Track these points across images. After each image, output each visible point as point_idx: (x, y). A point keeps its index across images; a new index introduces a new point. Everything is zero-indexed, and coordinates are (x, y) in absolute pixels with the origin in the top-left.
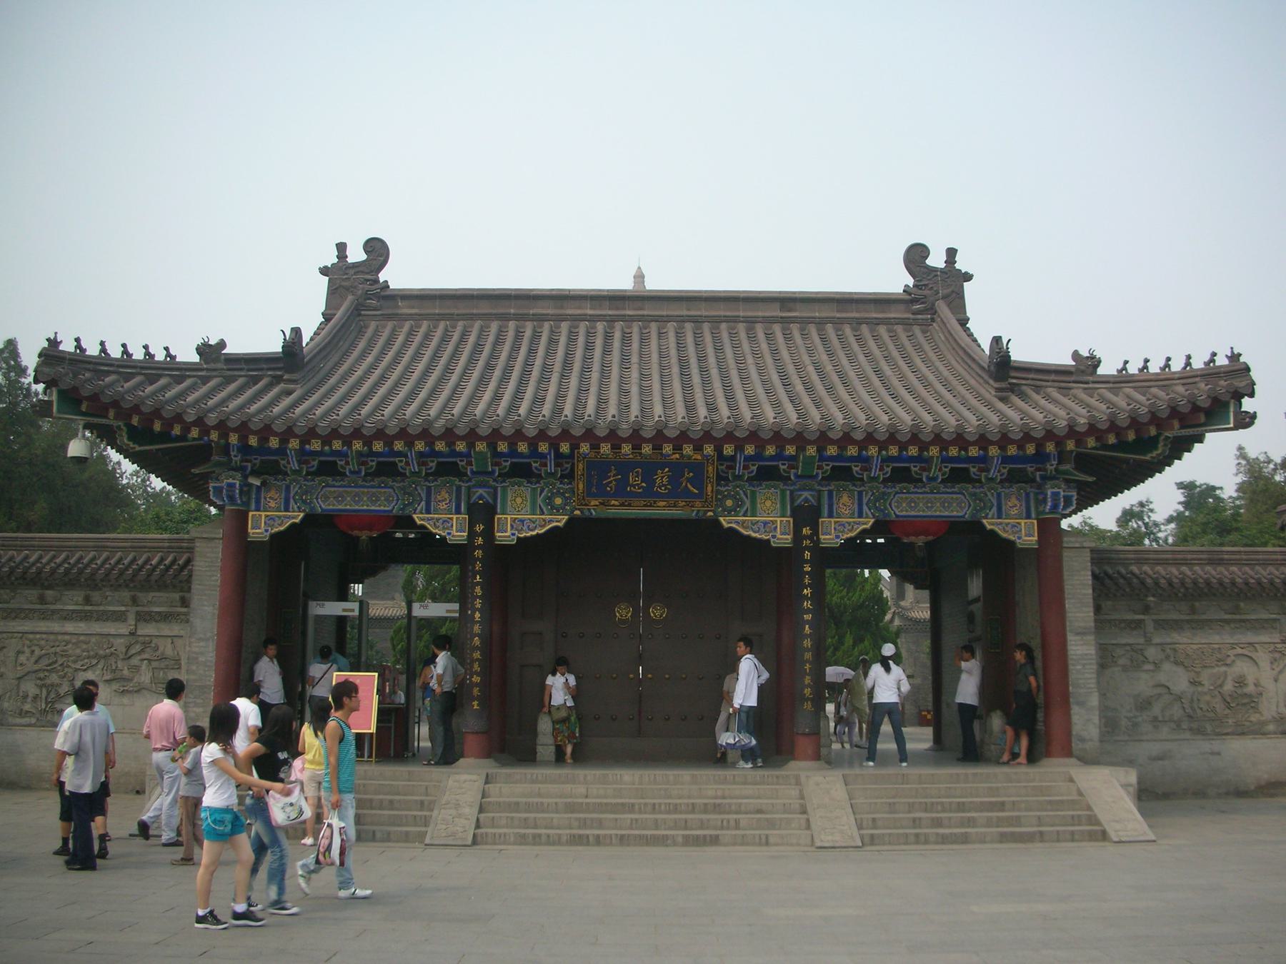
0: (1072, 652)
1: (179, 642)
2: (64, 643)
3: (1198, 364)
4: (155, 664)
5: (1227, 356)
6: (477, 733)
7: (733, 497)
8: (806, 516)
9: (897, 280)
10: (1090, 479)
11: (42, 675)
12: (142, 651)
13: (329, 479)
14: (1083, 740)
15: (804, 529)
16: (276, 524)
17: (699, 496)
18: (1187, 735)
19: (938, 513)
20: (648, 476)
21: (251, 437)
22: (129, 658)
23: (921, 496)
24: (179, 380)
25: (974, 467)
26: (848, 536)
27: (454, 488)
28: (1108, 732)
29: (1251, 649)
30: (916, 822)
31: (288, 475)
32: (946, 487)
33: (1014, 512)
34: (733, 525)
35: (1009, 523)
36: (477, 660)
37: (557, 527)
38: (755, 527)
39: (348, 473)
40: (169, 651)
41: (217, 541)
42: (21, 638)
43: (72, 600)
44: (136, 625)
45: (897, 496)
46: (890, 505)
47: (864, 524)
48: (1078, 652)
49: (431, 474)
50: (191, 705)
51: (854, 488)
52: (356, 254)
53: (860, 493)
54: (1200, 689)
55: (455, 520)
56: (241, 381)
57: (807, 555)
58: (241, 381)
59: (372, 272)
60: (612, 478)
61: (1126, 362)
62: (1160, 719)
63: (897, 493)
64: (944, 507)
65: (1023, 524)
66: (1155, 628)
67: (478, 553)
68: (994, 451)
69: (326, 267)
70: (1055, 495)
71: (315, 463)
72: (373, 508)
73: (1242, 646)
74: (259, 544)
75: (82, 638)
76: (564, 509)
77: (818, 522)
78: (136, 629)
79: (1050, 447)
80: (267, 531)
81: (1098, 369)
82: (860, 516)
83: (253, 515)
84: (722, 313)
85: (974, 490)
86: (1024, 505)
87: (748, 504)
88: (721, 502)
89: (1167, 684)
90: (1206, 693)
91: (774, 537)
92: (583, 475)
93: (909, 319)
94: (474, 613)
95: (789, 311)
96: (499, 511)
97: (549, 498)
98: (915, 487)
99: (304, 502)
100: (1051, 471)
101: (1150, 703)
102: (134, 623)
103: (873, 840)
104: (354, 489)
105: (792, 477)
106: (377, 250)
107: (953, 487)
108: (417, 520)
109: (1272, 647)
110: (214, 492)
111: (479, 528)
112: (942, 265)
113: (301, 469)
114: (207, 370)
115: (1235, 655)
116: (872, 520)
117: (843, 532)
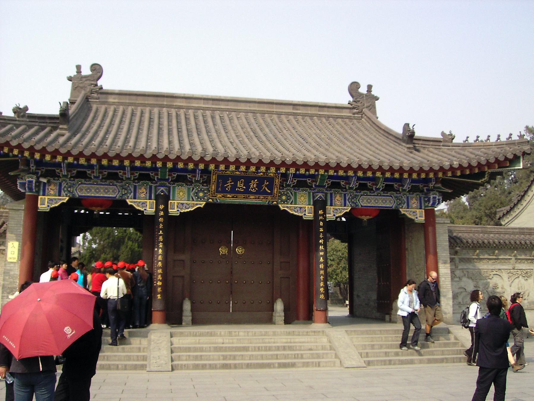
3: (503, 139)
5: (518, 136)
6: (160, 311)
7: (286, 195)
9: (345, 99)
10: (450, 191)
13: (83, 180)
14: (445, 313)
15: (320, 211)
16: (53, 203)
17: (271, 194)
19: (380, 205)
20: (247, 184)
21: (47, 155)
23: (373, 197)
25: (396, 184)
27: (148, 186)
29: (500, 272)
30: (386, 354)
31: (61, 178)
33: (414, 206)
34: (286, 209)
36: (160, 274)
37: (200, 207)
39: (92, 178)
41: (21, 211)
45: (362, 196)
46: (359, 200)
48: (443, 272)
49: (137, 179)
51: (342, 192)
52: (86, 71)
55: (148, 203)
56: (36, 128)
57: (321, 224)
58: (36, 128)
59: (94, 80)
60: (229, 184)
61: (468, 137)
62: (462, 303)
63: (362, 195)
64: (383, 203)
65: (418, 212)
67: (161, 220)
68: (406, 176)
69: (70, 77)
70: (434, 198)
71: (75, 172)
73: (496, 270)
74: (45, 214)
76: (204, 198)
79: (431, 175)
80: (48, 206)
81: (453, 140)
82: (345, 206)
84: (265, 109)
85: (397, 195)
87: (293, 198)
89: (464, 287)
91: (305, 215)
92: (215, 182)
93: (351, 116)
94: (158, 250)
95: (297, 110)
96: (171, 198)
97: (196, 193)
99: (69, 192)
100: (432, 187)
103: (369, 363)
104: (95, 186)
105: (314, 186)
109: (509, 271)
110: (20, 185)
111: (162, 207)
112: (366, 92)
113: (68, 175)
114: (19, 121)
115: (494, 275)
116: (350, 208)
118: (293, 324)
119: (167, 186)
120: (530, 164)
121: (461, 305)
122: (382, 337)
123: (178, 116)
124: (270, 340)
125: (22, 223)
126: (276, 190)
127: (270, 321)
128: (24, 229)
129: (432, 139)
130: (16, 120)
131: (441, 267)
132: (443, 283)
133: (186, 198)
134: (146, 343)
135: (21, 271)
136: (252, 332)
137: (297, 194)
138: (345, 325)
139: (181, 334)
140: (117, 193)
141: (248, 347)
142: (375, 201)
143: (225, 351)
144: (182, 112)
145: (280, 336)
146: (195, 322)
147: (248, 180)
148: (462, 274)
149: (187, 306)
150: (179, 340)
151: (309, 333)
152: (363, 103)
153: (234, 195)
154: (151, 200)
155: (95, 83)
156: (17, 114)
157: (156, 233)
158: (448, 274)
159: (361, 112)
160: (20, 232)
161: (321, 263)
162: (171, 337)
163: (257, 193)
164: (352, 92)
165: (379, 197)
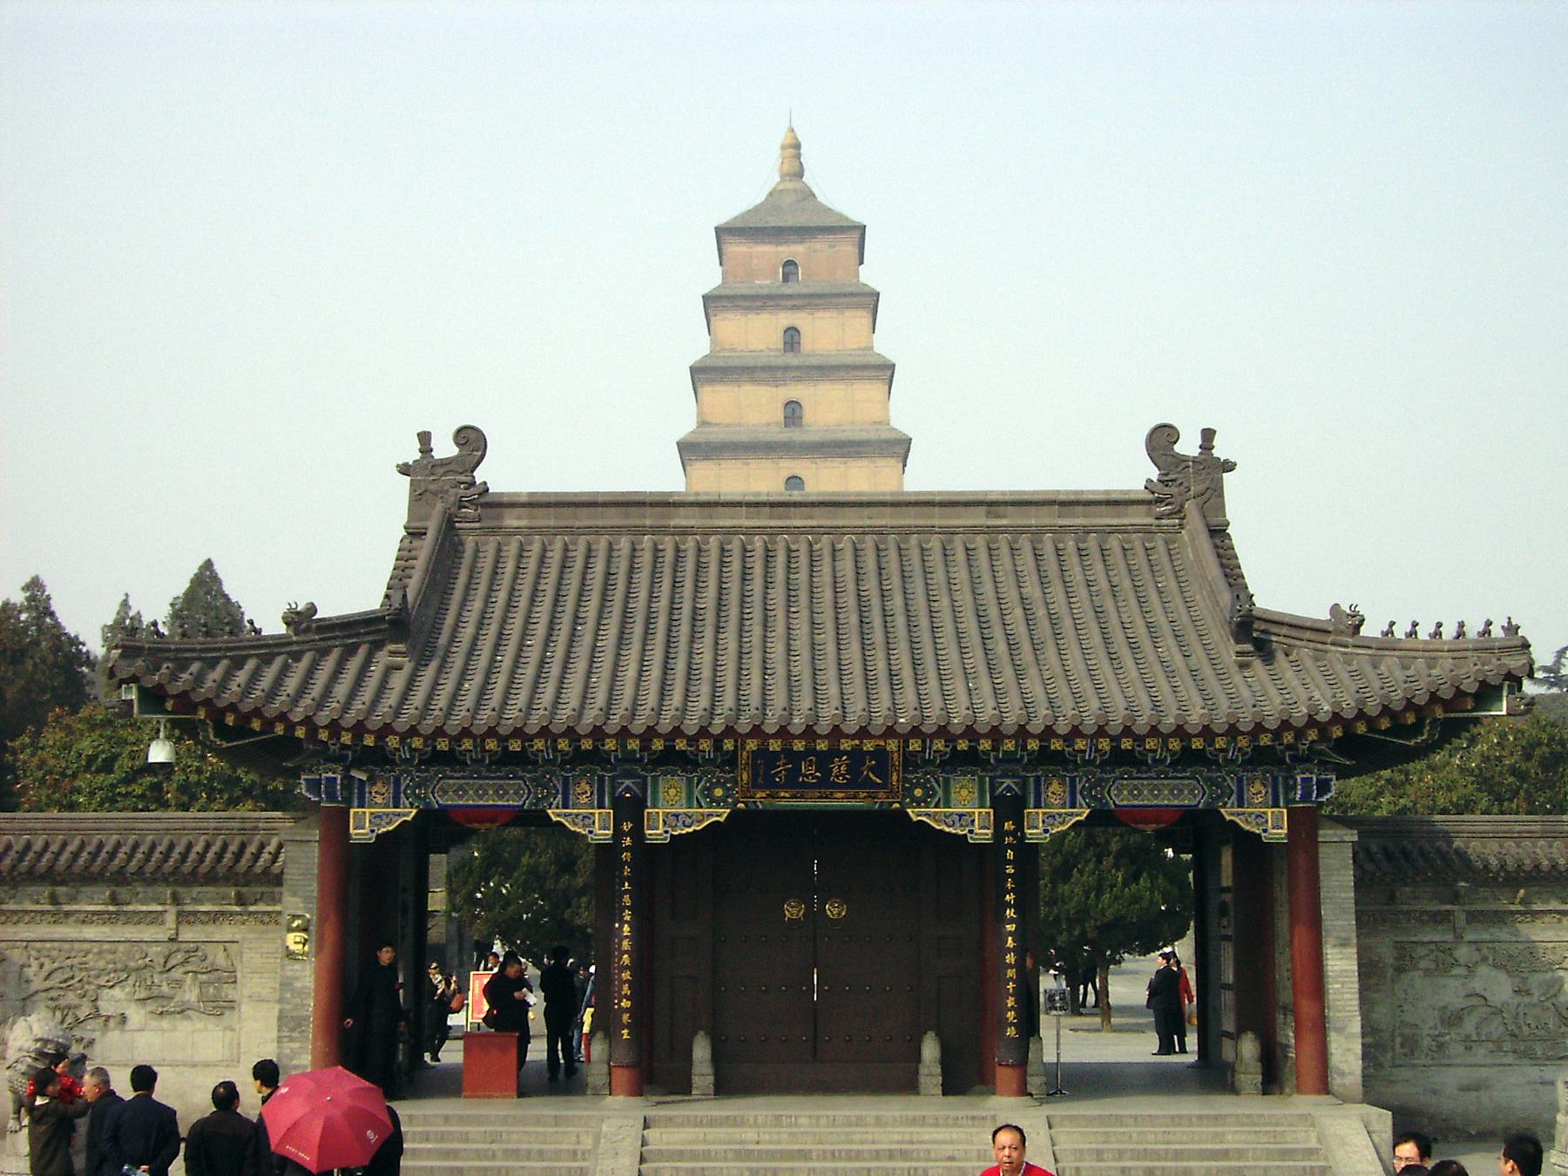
0: (1329, 968)
1: (232, 948)
2: (83, 953)
4: (204, 977)
5: (1503, 627)
6: (627, 1067)
7: (923, 786)
8: (1009, 809)
11: (53, 994)
12: (186, 961)
14: (1342, 1074)
18: (1510, 1059)
22: (170, 970)
24: (267, 660)
26: (1059, 829)
28: (1405, 1055)
31: (397, 765)
32: (1175, 771)
35: (1252, 813)
36: (627, 981)
38: (949, 821)
40: (221, 960)
41: (312, 844)
42: (26, 947)
43: (93, 901)
44: (177, 929)
47: (1077, 815)
48: (1336, 968)
50: (285, 1040)
52: (444, 448)
53: (1073, 780)
54: (1527, 1000)
55: (597, 815)
57: (1010, 854)
60: (782, 768)
64: (1173, 794)
66: (1469, 922)
67: (626, 856)
69: (406, 465)
72: (500, 803)
75: (106, 946)
77: (1023, 813)
78: (177, 934)
80: (373, 831)
81: (1362, 629)
82: (1073, 806)
83: (355, 813)
84: (912, 522)
86: (1270, 790)
88: (908, 792)
89: (1483, 993)
90: (1534, 1006)
91: (971, 832)
94: (621, 927)
97: (708, 789)
98: (1139, 772)
99: (418, 797)
101: (1460, 1018)
102: (174, 926)
106: (471, 441)
107: (1185, 771)
108: (552, 816)
114: (297, 642)
116: (1088, 811)
117: (1053, 824)
118: (970, 1095)
119: (639, 777)
120: (1526, 705)
121: (1472, 1044)
122: (1130, 1133)
123: (678, 552)
124: (864, 1137)
125: (316, 871)
126: (895, 777)
127: (908, 1085)
128: (321, 884)
129: (1308, 624)
130: (291, 644)
131: (1331, 954)
132: (1335, 997)
133: (684, 801)
134: (590, 1141)
135: (317, 980)
136: (827, 1117)
137: (952, 782)
138: (1154, 1094)
139: (670, 1121)
140: (526, 796)
141: (810, 1151)
142: (1151, 791)
143: (759, 1159)
144: (690, 544)
145: (893, 1126)
146: (725, 1087)
147: (824, 760)
148: (1476, 957)
149: (701, 1051)
150: (661, 1134)
151: (960, 1121)
152: (1185, 484)
153: (794, 791)
154: (604, 808)
155: (468, 479)
156: (292, 627)
157: (617, 887)
158: (1350, 974)
159: (1180, 511)
160: (313, 891)
161: (1009, 951)
162: (646, 1126)
163: (850, 784)
164: (1154, 455)
165: (1160, 782)
